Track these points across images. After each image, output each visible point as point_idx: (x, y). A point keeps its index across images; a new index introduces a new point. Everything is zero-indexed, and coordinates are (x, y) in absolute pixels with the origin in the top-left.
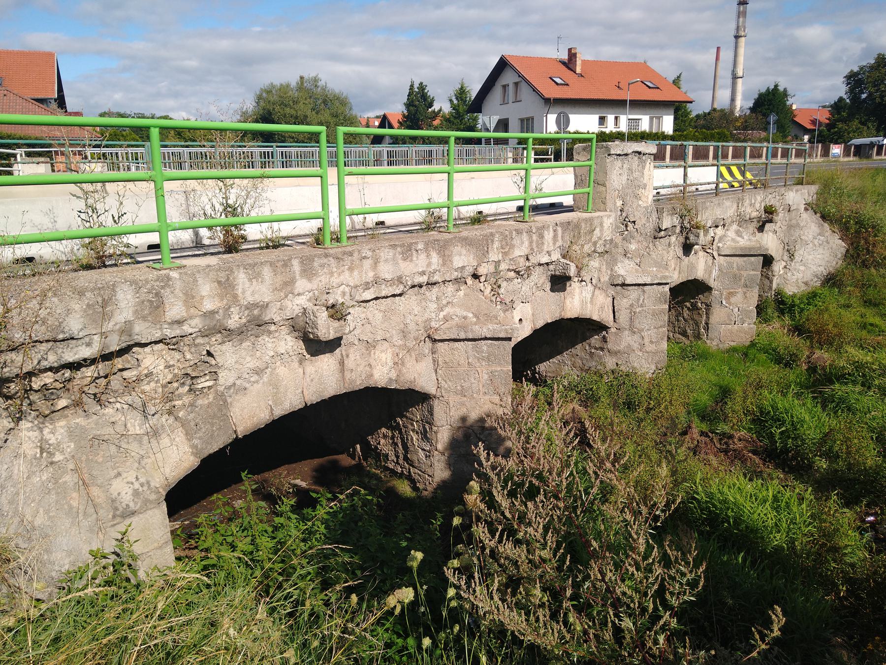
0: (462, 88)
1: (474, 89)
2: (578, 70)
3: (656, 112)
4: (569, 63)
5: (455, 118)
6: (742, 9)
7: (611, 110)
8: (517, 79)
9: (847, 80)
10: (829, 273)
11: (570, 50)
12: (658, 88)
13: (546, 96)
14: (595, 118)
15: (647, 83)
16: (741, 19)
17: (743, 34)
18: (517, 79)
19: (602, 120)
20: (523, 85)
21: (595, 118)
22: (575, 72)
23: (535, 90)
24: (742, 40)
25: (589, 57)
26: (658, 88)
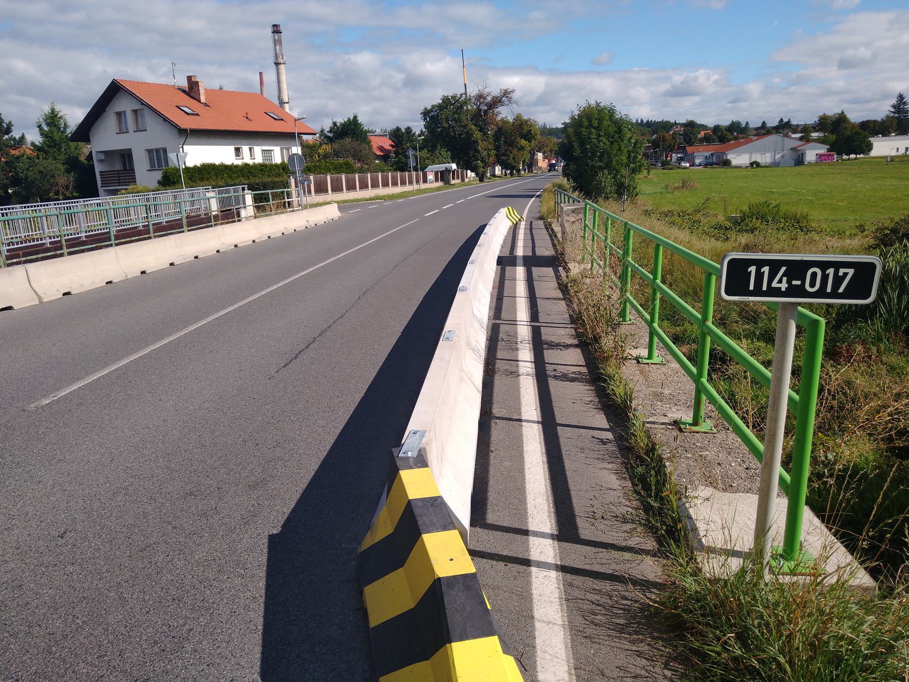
0: (53, 111)
1: (74, 116)
2: (203, 99)
3: (286, 143)
4: (192, 89)
5: (49, 146)
6: (276, 37)
7: (244, 141)
8: (137, 106)
9: (424, 116)
11: (189, 78)
12: (283, 120)
13: (183, 127)
14: (230, 149)
16: (278, 47)
17: (282, 61)
18: (137, 106)
19: (238, 151)
20: (147, 113)
21: (230, 149)
23: (166, 120)
24: (282, 67)
25: (215, 84)
26: (283, 120)
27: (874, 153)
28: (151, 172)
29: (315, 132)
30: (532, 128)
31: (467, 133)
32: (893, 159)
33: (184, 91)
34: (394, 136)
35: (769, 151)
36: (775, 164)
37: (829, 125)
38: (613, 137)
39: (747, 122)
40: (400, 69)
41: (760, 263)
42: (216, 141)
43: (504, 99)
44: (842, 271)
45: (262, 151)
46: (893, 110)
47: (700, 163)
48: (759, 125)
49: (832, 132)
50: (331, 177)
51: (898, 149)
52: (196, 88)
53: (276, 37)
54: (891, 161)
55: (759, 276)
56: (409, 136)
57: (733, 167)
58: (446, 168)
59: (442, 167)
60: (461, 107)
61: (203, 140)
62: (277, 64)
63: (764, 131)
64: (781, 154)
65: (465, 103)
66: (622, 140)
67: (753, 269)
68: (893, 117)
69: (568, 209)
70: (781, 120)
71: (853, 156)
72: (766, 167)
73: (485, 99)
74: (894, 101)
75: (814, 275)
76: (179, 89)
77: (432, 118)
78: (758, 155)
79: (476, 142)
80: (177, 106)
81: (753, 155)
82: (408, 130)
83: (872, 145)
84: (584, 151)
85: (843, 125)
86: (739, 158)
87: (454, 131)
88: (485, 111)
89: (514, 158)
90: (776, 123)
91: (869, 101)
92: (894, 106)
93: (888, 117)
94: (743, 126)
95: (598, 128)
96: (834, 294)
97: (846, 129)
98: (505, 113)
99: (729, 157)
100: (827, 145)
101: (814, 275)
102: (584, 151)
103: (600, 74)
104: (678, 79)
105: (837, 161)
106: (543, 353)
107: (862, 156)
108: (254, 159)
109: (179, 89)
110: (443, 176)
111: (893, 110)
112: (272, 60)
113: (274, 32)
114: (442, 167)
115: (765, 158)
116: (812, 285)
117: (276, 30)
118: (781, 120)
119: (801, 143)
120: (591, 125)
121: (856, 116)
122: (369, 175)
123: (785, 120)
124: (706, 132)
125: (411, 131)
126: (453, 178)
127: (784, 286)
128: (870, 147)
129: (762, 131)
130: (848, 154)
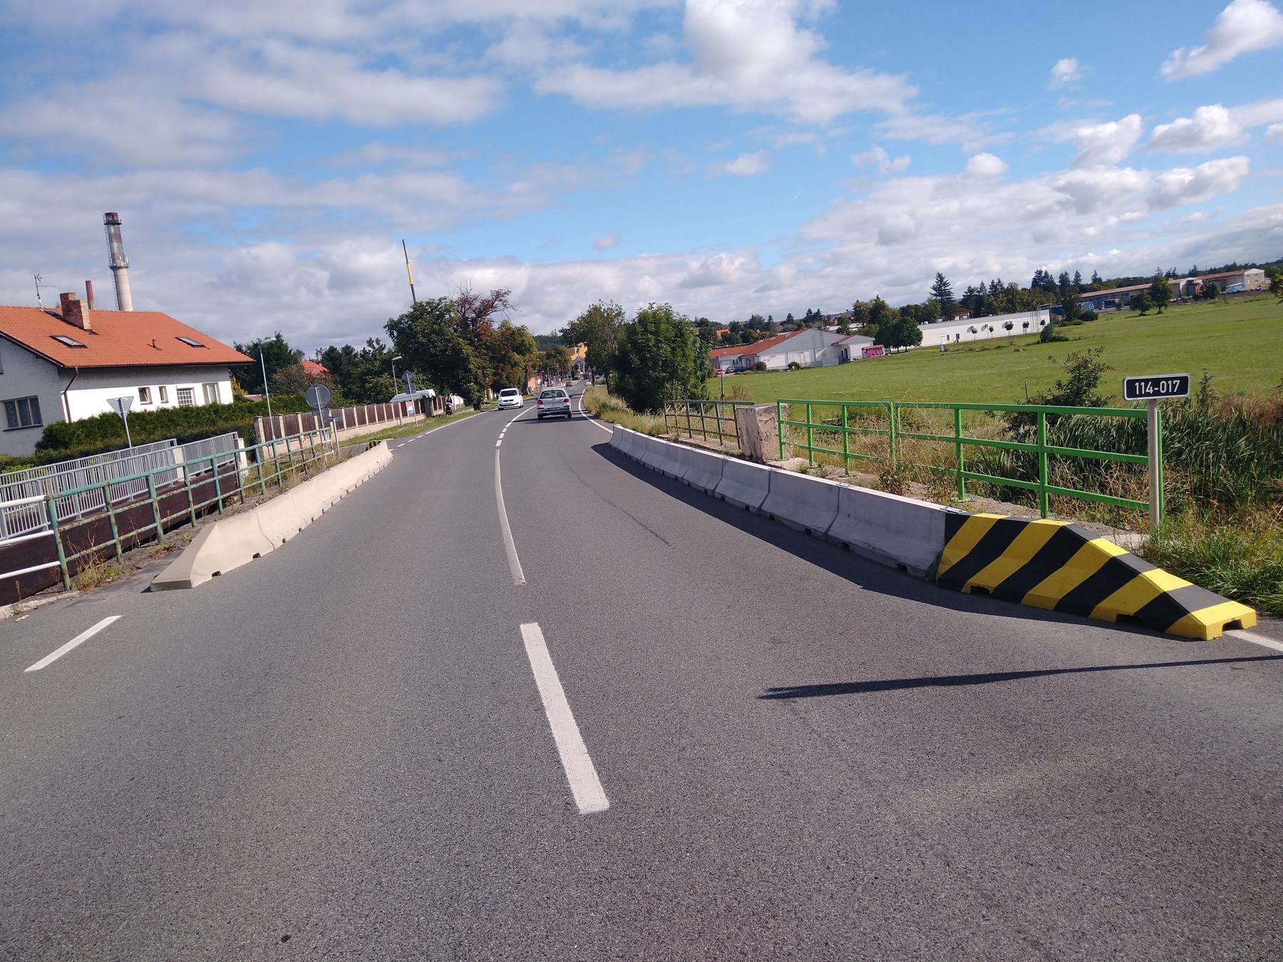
2: (87, 325)
3: (210, 377)
4: (69, 310)
6: (113, 230)
7: (152, 379)
10: (1257, 404)
12: (203, 346)
13: (68, 364)
14: (133, 391)
15: (183, 339)
16: (115, 245)
17: (123, 264)
19: (143, 392)
22: (82, 328)
23: (38, 356)
24: (123, 272)
26: (203, 346)
27: (924, 343)
28: (10, 434)
30: (524, 338)
31: (453, 348)
32: (946, 348)
33: (55, 315)
34: (326, 359)
35: (808, 349)
36: (816, 365)
37: (866, 314)
38: (674, 342)
39: (770, 316)
40: (323, 265)
41: (1140, 381)
42: (112, 381)
43: (496, 303)
44: (1175, 382)
45: (178, 390)
46: (934, 292)
48: (785, 319)
49: (872, 321)
50: (285, 419)
52: (76, 310)
53: (113, 230)
54: (946, 351)
55: (1140, 387)
56: (349, 359)
57: (769, 371)
58: (424, 397)
59: (419, 394)
60: (442, 316)
61: (94, 381)
62: (115, 268)
63: (792, 326)
64: (821, 352)
65: (448, 311)
66: (686, 345)
67: (1137, 384)
68: (935, 300)
70: (810, 311)
71: (902, 348)
72: (806, 368)
73: (470, 304)
74: (933, 282)
75: (1163, 384)
76: (48, 313)
77: (401, 331)
78: (795, 355)
79: (467, 359)
80: (51, 337)
81: (790, 355)
82: (348, 350)
83: (921, 333)
84: (643, 360)
85: (883, 313)
86: (774, 360)
87: (435, 347)
88: (474, 321)
89: (508, 378)
90: (803, 316)
91: (913, 282)
92: (934, 288)
93: (929, 300)
94: (766, 321)
95: (656, 333)
96: (1173, 393)
97: (887, 317)
98: (496, 320)
99: (762, 359)
100: (871, 337)
101: (1163, 384)
102: (643, 360)
103: (598, 262)
104: (695, 265)
105: (886, 354)
106: (521, 644)
107: (912, 347)
108: (167, 402)
109: (48, 313)
110: (424, 406)
111: (934, 292)
112: (107, 262)
113: (108, 223)
114: (419, 394)
115: (804, 358)
116: (1163, 390)
117: (111, 220)
118: (810, 311)
119: (841, 337)
120: (646, 330)
121: (895, 300)
122: (343, 410)
123: (814, 311)
124: (723, 331)
125: (352, 352)
126: (435, 409)
127: (1151, 391)
128: (919, 337)
129: (790, 326)
130: (896, 346)
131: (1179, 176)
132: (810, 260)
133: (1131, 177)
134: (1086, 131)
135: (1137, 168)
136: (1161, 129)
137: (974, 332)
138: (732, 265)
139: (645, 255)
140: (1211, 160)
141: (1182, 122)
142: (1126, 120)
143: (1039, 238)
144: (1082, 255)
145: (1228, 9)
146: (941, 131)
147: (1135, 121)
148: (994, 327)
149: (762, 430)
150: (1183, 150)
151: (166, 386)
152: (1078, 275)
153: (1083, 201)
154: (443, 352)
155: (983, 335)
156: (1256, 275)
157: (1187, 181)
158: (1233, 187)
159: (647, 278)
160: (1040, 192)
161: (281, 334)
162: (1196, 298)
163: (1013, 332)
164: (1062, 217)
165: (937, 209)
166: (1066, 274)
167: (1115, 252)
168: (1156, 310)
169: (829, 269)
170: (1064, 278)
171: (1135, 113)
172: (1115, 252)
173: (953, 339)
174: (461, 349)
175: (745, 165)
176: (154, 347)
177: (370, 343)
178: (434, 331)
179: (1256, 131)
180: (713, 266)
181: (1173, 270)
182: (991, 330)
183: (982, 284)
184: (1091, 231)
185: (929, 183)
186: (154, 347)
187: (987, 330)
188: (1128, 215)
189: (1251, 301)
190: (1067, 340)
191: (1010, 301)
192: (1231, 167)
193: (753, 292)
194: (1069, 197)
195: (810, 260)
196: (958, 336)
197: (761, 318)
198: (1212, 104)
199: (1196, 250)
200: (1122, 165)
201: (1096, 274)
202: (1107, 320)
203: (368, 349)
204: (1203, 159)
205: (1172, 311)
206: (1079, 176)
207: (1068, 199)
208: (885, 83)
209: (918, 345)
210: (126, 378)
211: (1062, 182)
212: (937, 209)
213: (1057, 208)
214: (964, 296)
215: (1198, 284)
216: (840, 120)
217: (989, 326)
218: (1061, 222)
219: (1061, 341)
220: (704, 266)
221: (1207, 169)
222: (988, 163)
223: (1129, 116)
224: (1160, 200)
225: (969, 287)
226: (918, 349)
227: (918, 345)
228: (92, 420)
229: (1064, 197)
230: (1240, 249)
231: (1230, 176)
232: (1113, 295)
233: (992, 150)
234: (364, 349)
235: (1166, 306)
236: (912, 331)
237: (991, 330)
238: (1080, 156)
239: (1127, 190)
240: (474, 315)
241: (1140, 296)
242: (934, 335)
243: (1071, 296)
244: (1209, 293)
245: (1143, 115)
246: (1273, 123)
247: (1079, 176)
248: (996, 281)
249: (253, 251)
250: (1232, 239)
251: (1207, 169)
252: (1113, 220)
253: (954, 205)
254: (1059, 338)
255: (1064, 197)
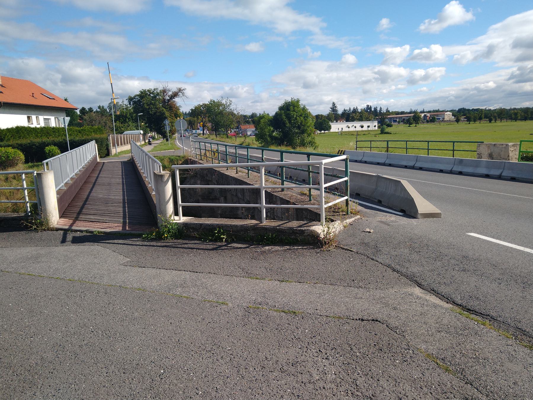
7: (33, 112)
12: (54, 99)
14: (25, 117)
21: (25, 117)
26: (54, 99)
27: (332, 130)
29: (76, 108)
40: (59, 71)
45: (44, 119)
47: (251, 134)
51: (338, 128)
54: (341, 134)
61: (7, 110)
69: (511, 145)
71: (323, 132)
74: (331, 106)
88: (168, 100)
104: (227, 89)
107: (327, 131)
108: (39, 124)
128: (330, 128)
131: (420, 73)
132: (275, 92)
133: (403, 72)
134: (388, 50)
135: (405, 67)
136: (417, 52)
137: (349, 128)
138: (243, 91)
139: (206, 82)
140: (432, 67)
141: (425, 50)
142: (404, 47)
143: (365, 92)
144: (380, 101)
145: (447, 6)
146: (333, 43)
147: (407, 47)
148: (356, 126)
149: (511, 155)
150: (424, 62)
151: (39, 116)
152: (381, 108)
153: (383, 78)
154: (155, 113)
155: (352, 129)
156: (449, 114)
157: (422, 75)
158: (439, 79)
159: (206, 92)
160: (367, 73)
161: (67, 99)
162: (428, 122)
163: (364, 129)
164: (375, 84)
165: (328, 75)
166: (377, 107)
167: (392, 100)
168: (415, 125)
169: (282, 96)
170: (375, 109)
171: (408, 44)
172: (392, 100)
173: (340, 130)
174: (164, 113)
175: (253, 47)
176: (33, 97)
177: (99, 107)
178: (151, 104)
179: (450, 57)
180: (235, 90)
181: (416, 110)
182: (355, 127)
183: (350, 108)
184: (385, 91)
185: (326, 64)
186: (33, 97)
187: (354, 127)
188: (400, 86)
189: (449, 125)
190: (391, 134)
191: (361, 116)
192: (439, 71)
193: (250, 103)
194: (378, 76)
195: (275, 92)
196: (342, 129)
197: (256, 114)
198: (437, 44)
199: (422, 103)
200: (400, 66)
201: (388, 109)
202: (396, 127)
203: (98, 110)
204: (430, 66)
205: (421, 126)
206: (384, 68)
207: (378, 77)
208: (314, 20)
209: (329, 131)
210: (21, 110)
211: (376, 70)
212: (328, 75)
213: (373, 80)
214: (342, 112)
215: (428, 116)
216: (294, 33)
217: (355, 126)
218: (373, 87)
219: (389, 134)
220: (231, 89)
221: (431, 71)
222: (350, 58)
223: (405, 46)
224: (412, 81)
225: (344, 109)
226: (329, 133)
227: (329, 131)
228: (12, 128)
229: (377, 76)
230: (437, 104)
231: (438, 75)
232: (396, 118)
233: (352, 53)
234: (97, 110)
235: (418, 124)
236: (327, 125)
237: (355, 127)
238: (384, 60)
239: (400, 76)
240: (168, 98)
241: (409, 119)
242: (336, 127)
243: (384, 116)
244: (432, 120)
245: (411, 46)
246: (456, 55)
247: (384, 68)
248: (355, 107)
249: (25, 61)
250: (435, 100)
251: (431, 71)
252: (393, 87)
253: (335, 75)
254: (388, 132)
255: (377, 76)
